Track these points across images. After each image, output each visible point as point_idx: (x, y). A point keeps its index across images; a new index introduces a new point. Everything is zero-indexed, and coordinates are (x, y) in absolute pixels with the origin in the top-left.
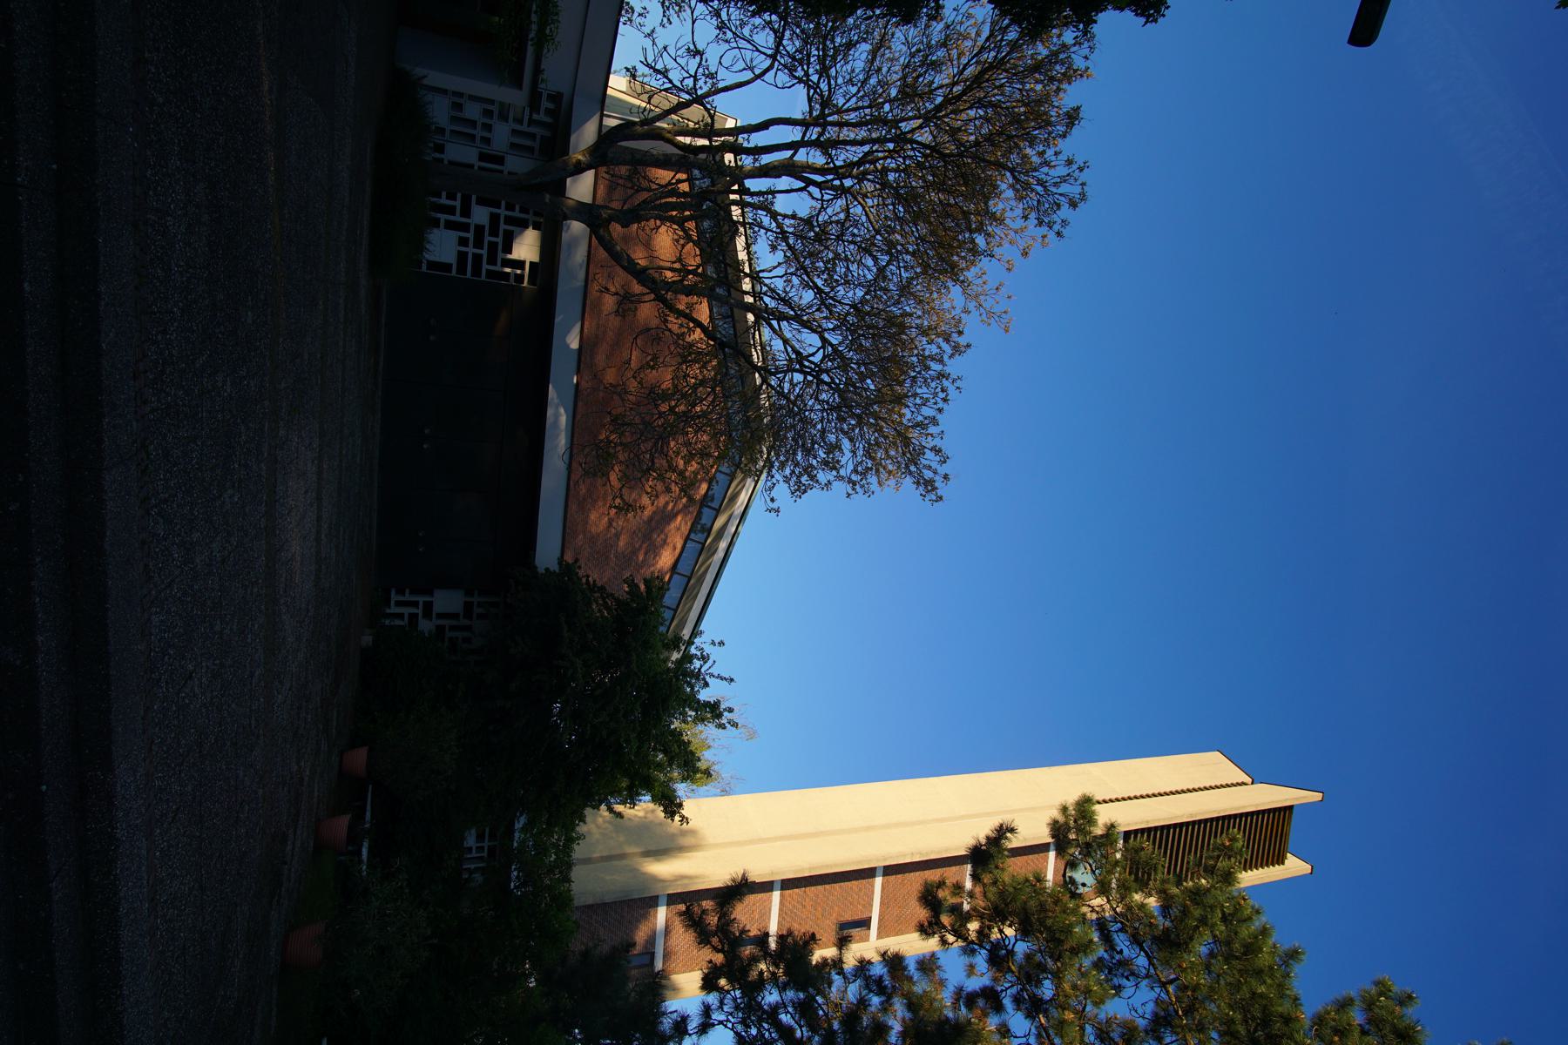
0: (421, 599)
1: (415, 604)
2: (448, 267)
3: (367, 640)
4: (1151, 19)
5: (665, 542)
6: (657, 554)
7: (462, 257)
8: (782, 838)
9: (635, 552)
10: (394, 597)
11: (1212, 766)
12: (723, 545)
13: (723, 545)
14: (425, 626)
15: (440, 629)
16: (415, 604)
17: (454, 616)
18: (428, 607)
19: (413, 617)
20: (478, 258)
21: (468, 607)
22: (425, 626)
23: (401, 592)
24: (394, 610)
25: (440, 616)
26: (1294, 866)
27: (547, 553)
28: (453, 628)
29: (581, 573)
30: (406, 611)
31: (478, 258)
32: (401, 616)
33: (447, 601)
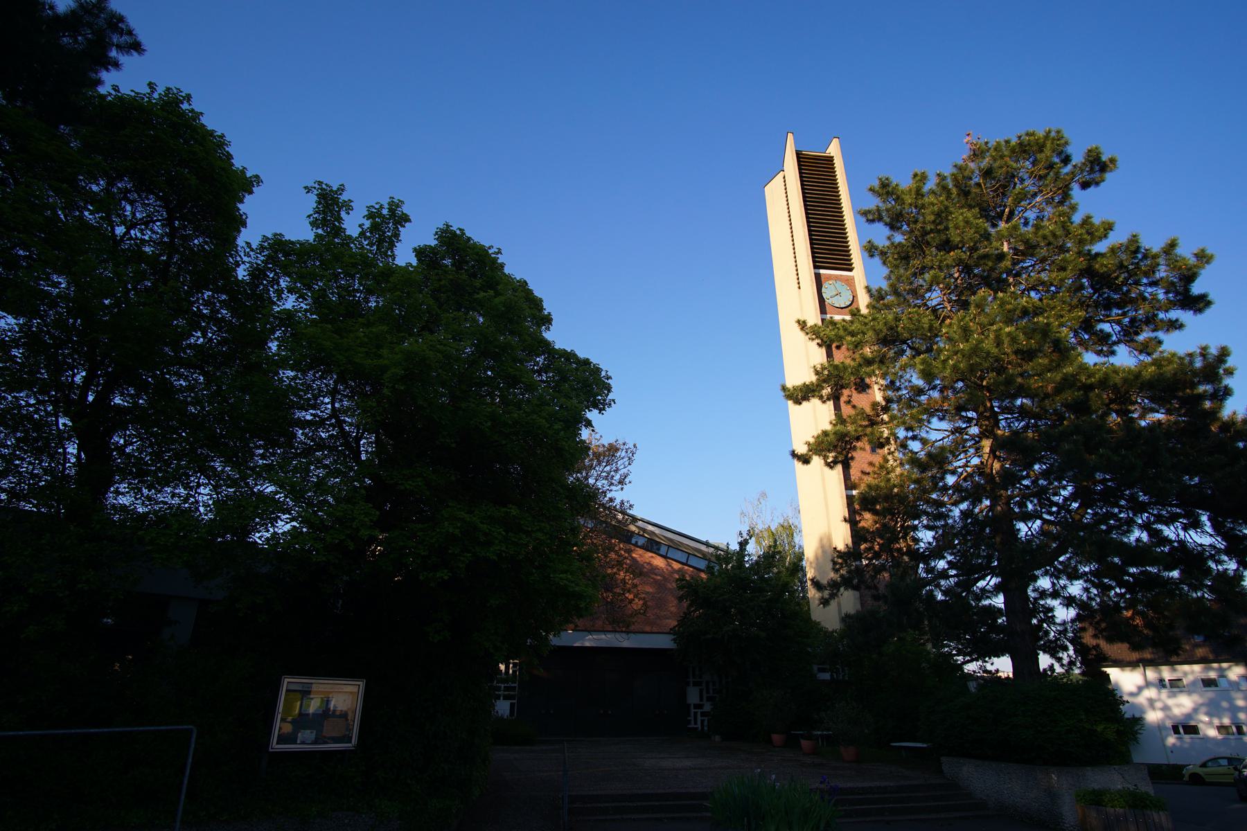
0: (693, 711)
1: (695, 714)
2: (512, 705)
3: (717, 738)
4: (244, 225)
5: (649, 564)
6: (657, 568)
7: (506, 698)
8: (825, 498)
9: (656, 581)
10: (692, 725)
11: (773, 191)
12: (650, 528)
13: (650, 528)
14: (707, 707)
15: (709, 699)
16: (695, 714)
17: (701, 691)
18: (696, 706)
19: (703, 714)
20: (507, 689)
21: (695, 684)
22: (707, 707)
23: (689, 722)
24: (699, 725)
25: (701, 699)
26: (834, 150)
27: (664, 642)
28: (708, 692)
29: (454, 228)
30: (699, 718)
31: (507, 689)
32: (702, 721)
33: (693, 696)
